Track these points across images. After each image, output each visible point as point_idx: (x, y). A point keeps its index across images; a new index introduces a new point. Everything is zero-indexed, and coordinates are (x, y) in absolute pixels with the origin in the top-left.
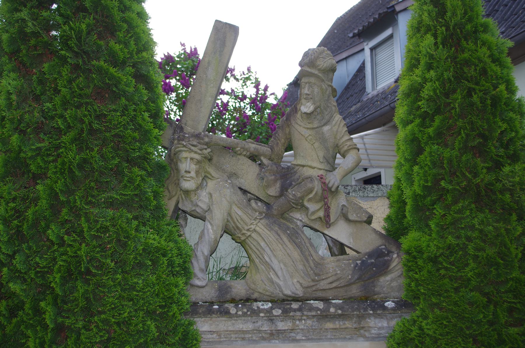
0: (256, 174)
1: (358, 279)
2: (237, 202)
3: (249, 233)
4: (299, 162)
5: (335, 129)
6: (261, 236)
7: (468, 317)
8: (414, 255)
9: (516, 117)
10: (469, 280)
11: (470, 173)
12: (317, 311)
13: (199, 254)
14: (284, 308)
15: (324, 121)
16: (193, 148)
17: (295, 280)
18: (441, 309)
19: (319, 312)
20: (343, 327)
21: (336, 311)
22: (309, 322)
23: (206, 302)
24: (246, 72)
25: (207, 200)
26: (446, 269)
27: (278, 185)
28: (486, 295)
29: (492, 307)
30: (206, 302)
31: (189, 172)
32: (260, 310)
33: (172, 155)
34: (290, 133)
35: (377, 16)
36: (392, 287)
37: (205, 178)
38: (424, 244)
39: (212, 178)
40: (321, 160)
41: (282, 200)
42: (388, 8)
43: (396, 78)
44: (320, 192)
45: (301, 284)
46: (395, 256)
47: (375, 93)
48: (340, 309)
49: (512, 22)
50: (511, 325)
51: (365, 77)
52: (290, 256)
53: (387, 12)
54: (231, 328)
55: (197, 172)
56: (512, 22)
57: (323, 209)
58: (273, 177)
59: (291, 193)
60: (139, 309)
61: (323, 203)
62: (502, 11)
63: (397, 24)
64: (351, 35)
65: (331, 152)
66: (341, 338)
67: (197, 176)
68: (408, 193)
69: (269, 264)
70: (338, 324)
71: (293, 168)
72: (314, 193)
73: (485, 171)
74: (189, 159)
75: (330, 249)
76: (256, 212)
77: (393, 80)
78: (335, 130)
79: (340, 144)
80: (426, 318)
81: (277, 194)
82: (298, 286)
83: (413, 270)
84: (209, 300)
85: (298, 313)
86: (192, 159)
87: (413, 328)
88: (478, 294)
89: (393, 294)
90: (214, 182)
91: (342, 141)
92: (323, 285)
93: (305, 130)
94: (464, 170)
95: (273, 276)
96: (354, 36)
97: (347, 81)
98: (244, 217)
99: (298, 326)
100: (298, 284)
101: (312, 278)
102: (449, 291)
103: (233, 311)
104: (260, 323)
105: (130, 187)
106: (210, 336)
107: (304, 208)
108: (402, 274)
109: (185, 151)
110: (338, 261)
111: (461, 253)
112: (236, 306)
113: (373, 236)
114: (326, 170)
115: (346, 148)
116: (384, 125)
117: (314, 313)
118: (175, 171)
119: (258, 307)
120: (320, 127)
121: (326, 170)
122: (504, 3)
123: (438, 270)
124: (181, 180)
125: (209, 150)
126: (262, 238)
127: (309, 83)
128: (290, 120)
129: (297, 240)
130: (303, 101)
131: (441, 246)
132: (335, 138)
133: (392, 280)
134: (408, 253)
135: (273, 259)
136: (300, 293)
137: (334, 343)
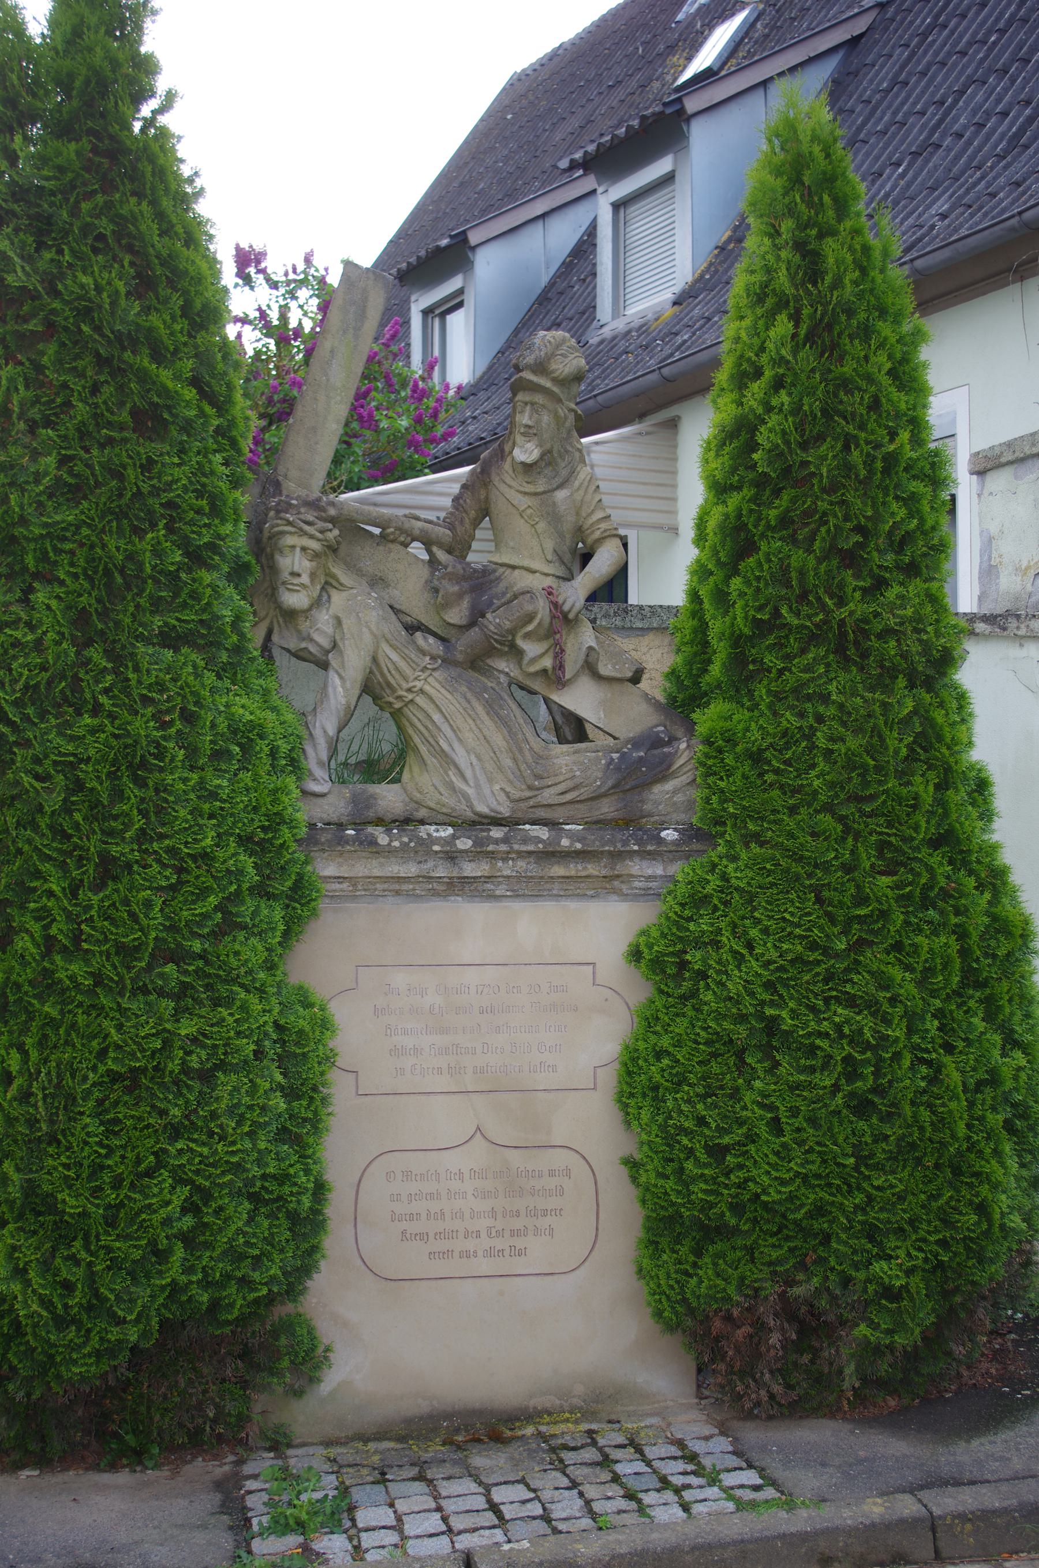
0: (423, 580)
1: (614, 787)
2: (389, 636)
3: (410, 697)
4: (505, 560)
5: (578, 497)
6: (434, 702)
7: (810, 858)
8: (719, 745)
9: (925, 490)
10: (815, 793)
11: (831, 598)
12: (536, 844)
13: (318, 732)
14: (476, 836)
15: (558, 480)
16: (306, 528)
17: (497, 787)
18: (762, 844)
19: (541, 846)
20: (584, 874)
21: (572, 844)
22: (521, 864)
23: (329, 824)
24: (301, 267)
25: (329, 630)
26: (777, 772)
27: (465, 603)
28: (841, 819)
29: (850, 840)
30: (329, 824)
31: (299, 575)
32: (432, 840)
33: (264, 540)
34: (487, 499)
35: (635, 123)
36: (675, 804)
37: (326, 586)
38: (740, 727)
39: (341, 587)
40: (549, 557)
41: (474, 633)
42: (665, 105)
43: (677, 289)
44: (547, 620)
45: (507, 794)
46: (683, 746)
47: (620, 325)
48: (579, 841)
49: (968, 191)
50: (882, 873)
51: (595, 275)
52: (488, 742)
53: (662, 113)
54: (377, 872)
55: (313, 575)
56: (968, 191)
57: (551, 654)
58: (456, 588)
59: (493, 620)
60: (226, 833)
61: (551, 641)
62: (949, 150)
63: (687, 147)
64: (564, 164)
65: (568, 542)
66: (578, 895)
67: (312, 581)
68: (716, 626)
69: (446, 755)
70: (573, 869)
71: (494, 571)
72: (535, 622)
73: (858, 595)
74: (298, 550)
75: (557, 729)
76: (424, 655)
77: (667, 296)
78: (579, 498)
79: (586, 527)
80: (734, 859)
81: (464, 622)
82: (502, 797)
83: (715, 774)
84: (335, 820)
85: (503, 847)
86: (304, 549)
87: (710, 877)
88: (828, 817)
89: (675, 817)
90: (345, 594)
91: (590, 521)
92: (548, 796)
93: (520, 496)
94: (821, 591)
95: (454, 779)
96: (573, 166)
97: (545, 279)
98: (402, 664)
99: (500, 870)
100: (502, 794)
101: (529, 783)
102: (778, 812)
103: (383, 840)
104: (431, 864)
105: (193, 606)
106: (338, 886)
107: (517, 653)
108: (694, 780)
109: (291, 533)
110: (575, 752)
111: (804, 744)
112: (388, 831)
113: (644, 707)
114: (558, 577)
115: (597, 535)
116: (642, 416)
117: (531, 848)
118: (267, 571)
119: (429, 835)
120: (549, 491)
121: (558, 577)
122: (956, 127)
123: (761, 775)
124: (282, 589)
125: (336, 532)
126: (437, 706)
127: (532, 404)
128: (489, 475)
129: (501, 712)
130: (519, 439)
131: (771, 731)
132: (578, 514)
133: (675, 792)
134: (708, 742)
135: (456, 745)
136: (505, 810)
137: (564, 903)
